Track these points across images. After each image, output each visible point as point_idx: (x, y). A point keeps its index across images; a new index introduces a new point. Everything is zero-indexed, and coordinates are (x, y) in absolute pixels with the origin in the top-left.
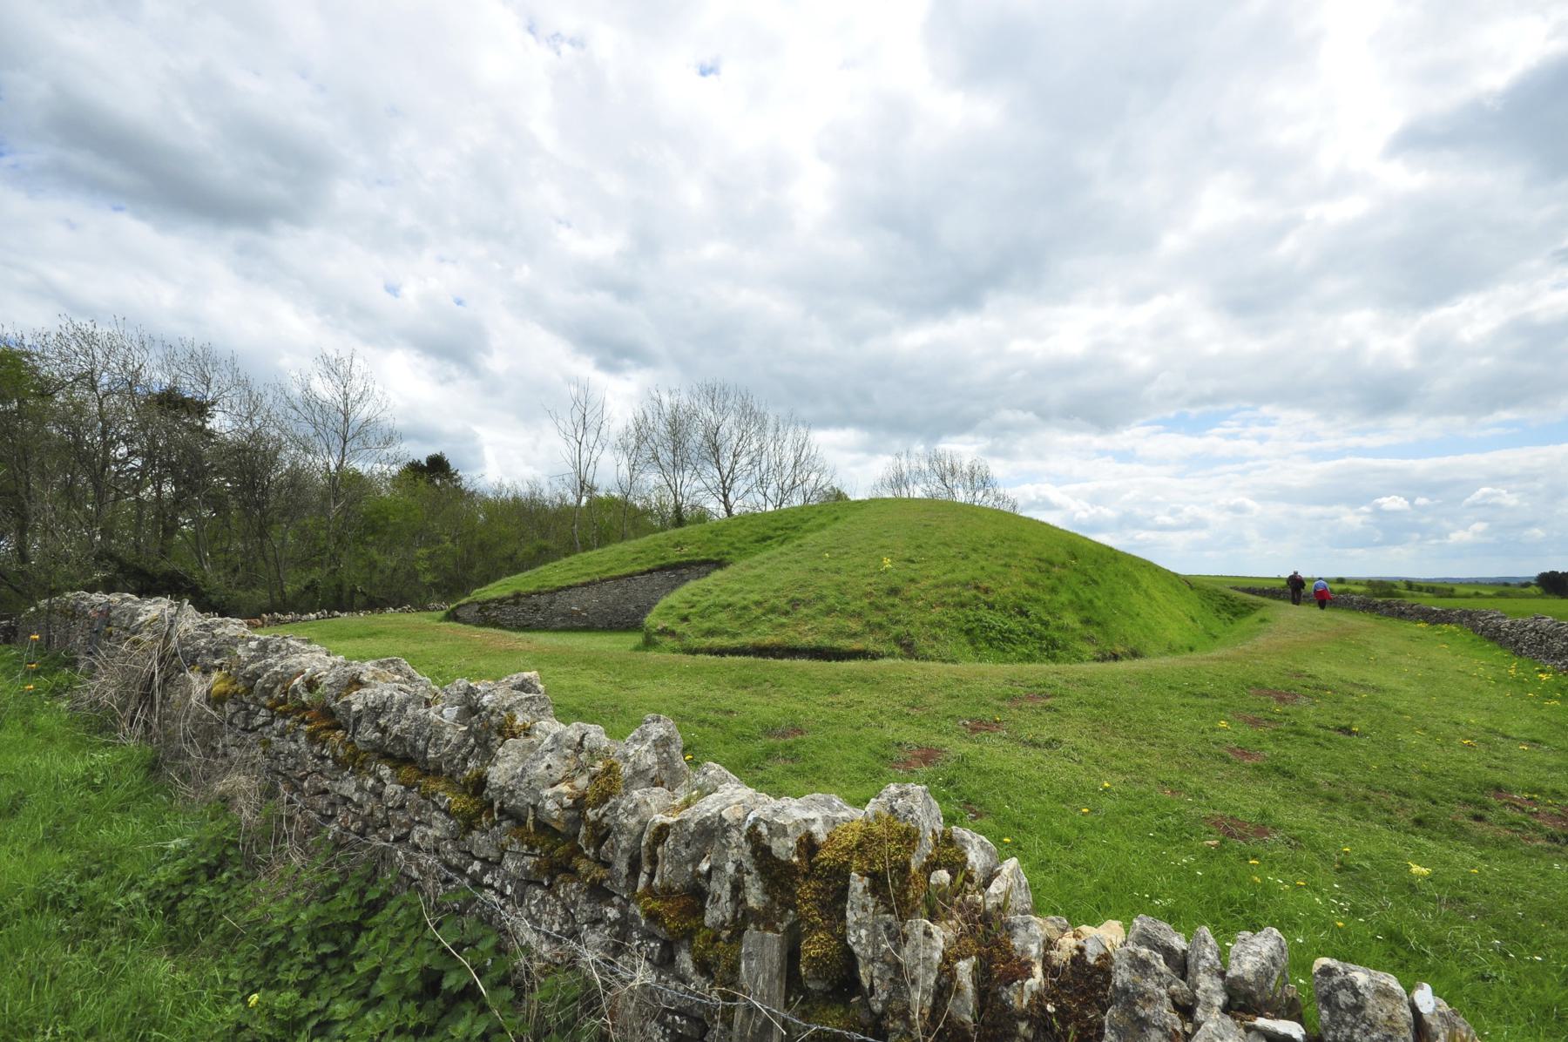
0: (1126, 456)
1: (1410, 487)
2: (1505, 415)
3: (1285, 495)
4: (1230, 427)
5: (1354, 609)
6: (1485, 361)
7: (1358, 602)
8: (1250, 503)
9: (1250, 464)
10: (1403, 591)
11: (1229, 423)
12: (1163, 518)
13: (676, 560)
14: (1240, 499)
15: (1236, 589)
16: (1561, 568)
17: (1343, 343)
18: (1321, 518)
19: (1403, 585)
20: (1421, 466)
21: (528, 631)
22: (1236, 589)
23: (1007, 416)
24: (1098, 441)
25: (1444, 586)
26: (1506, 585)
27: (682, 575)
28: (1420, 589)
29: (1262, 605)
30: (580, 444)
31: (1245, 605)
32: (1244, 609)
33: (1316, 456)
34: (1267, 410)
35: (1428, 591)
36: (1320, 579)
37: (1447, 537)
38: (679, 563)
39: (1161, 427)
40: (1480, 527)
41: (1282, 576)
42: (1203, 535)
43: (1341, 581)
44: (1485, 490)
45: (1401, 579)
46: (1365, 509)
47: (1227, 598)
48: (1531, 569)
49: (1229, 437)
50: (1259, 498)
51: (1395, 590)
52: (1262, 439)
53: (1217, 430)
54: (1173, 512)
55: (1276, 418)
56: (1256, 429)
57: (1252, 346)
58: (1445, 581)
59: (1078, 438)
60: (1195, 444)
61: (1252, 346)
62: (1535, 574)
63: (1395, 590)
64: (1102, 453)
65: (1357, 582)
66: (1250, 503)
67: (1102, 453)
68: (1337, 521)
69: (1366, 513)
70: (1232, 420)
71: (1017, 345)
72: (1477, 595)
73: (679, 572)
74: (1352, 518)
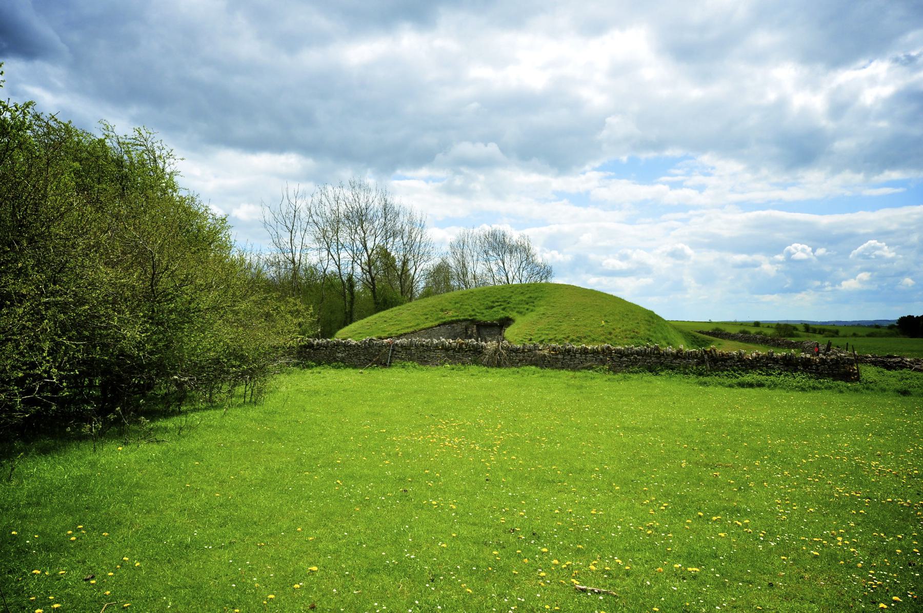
0: (582, 199)
1: (817, 238)
2: (895, 175)
3: (715, 243)
4: (677, 175)
5: (757, 343)
6: (883, 124)
7: (759, 339)
8: (688, 251)
9: (691, 212)
10: (800, 333)
11: (677, 172)
12: (613, 263)
13: (450, 319)
14: (680, 246)
15: (697, 332)
16: (916, 314)
17: (772, 96)
18: (744, 265)
19: (802, 328)
20: (825, 221)
21: (748, 342)
22: (700, 332)
23: (466, 149)
24: (558, 183)
25: (48, 441)
26: (877, 327)
27: (454, 327)
28: (814, 331)
29: (712, 341)
30: (291, 232)
31: (703, 341)
32: (703, 343)
33: (745, 206)
34: (706, 159)
35: (820, 333)
36: (731, 386)
37: (840, 285)
38: (452, 320)
39: (613, 174)
40: (864, 276)
41: (713, 321)
42: (648, 280)
43: (757, 324)
44: (872, 242)
45: (801, 322)
46: (780, 257)
47: (695, 337)
48: (894, 314)
49: (674, 185)
50: (695, 245)
51: (795, 332)
52: (701, 188)
53: (664, 179)
54: (624, 257)
55: (713, 168)
56: (698, 179)
57: (695, 93)
58: (834, 324)
59: (534, 178)
60: (644, 191)
61: (695, 93)
62: (897, 318)
63: (795, 332)
64: (560, 195)
65: (769, 325)
66: (688, 251)
67: (560, 195)
68: (757, 269)
69: (779, 262)
70: (679, 168)
71: (479, 72)
72: (855, 335)
73: (452, 325)
74: (768, 267)
